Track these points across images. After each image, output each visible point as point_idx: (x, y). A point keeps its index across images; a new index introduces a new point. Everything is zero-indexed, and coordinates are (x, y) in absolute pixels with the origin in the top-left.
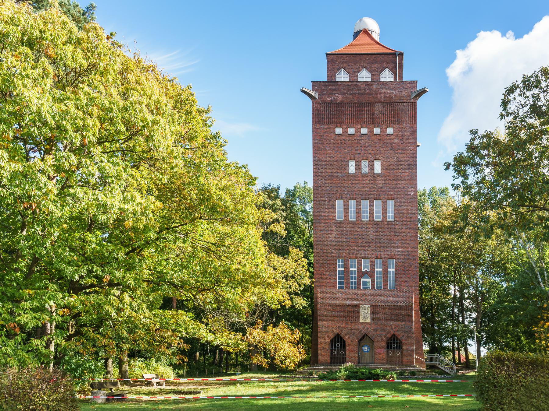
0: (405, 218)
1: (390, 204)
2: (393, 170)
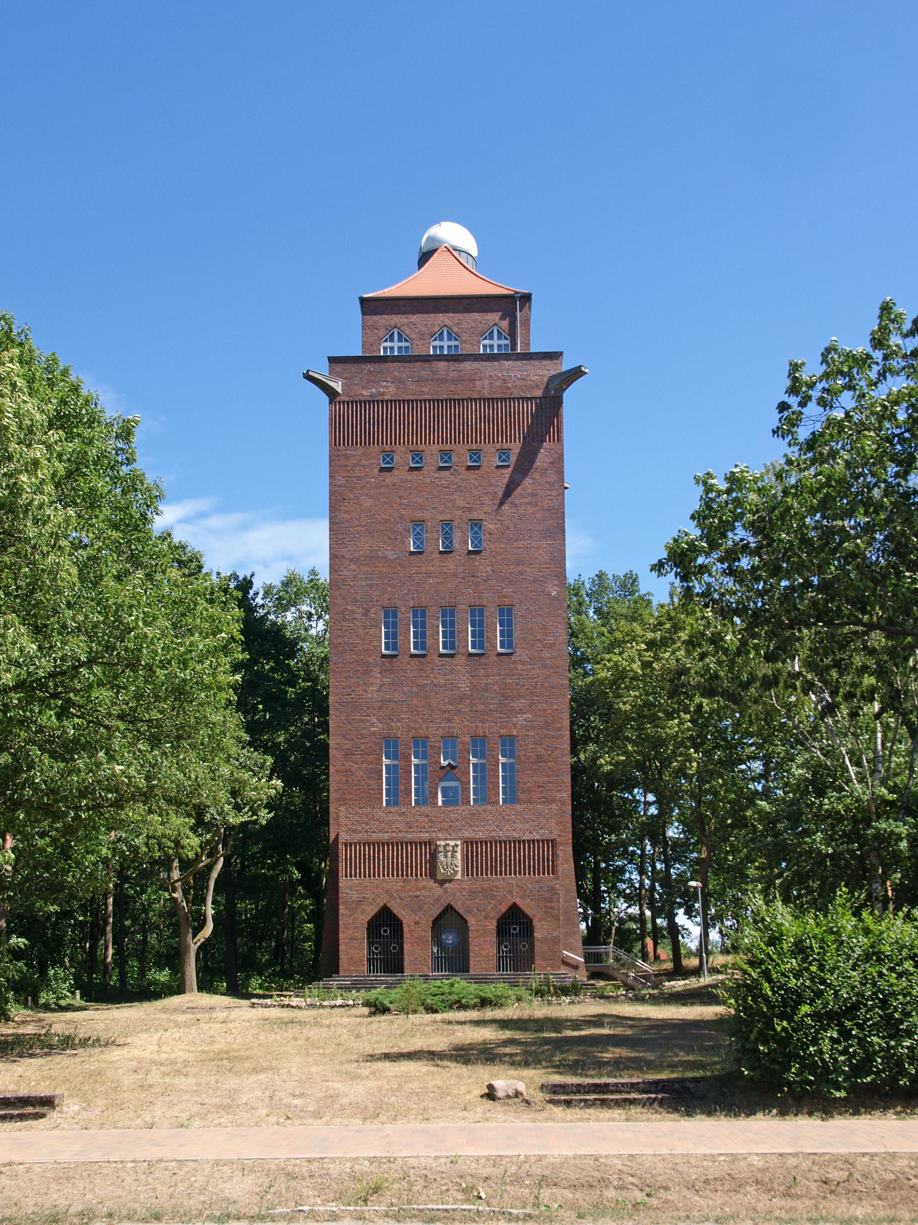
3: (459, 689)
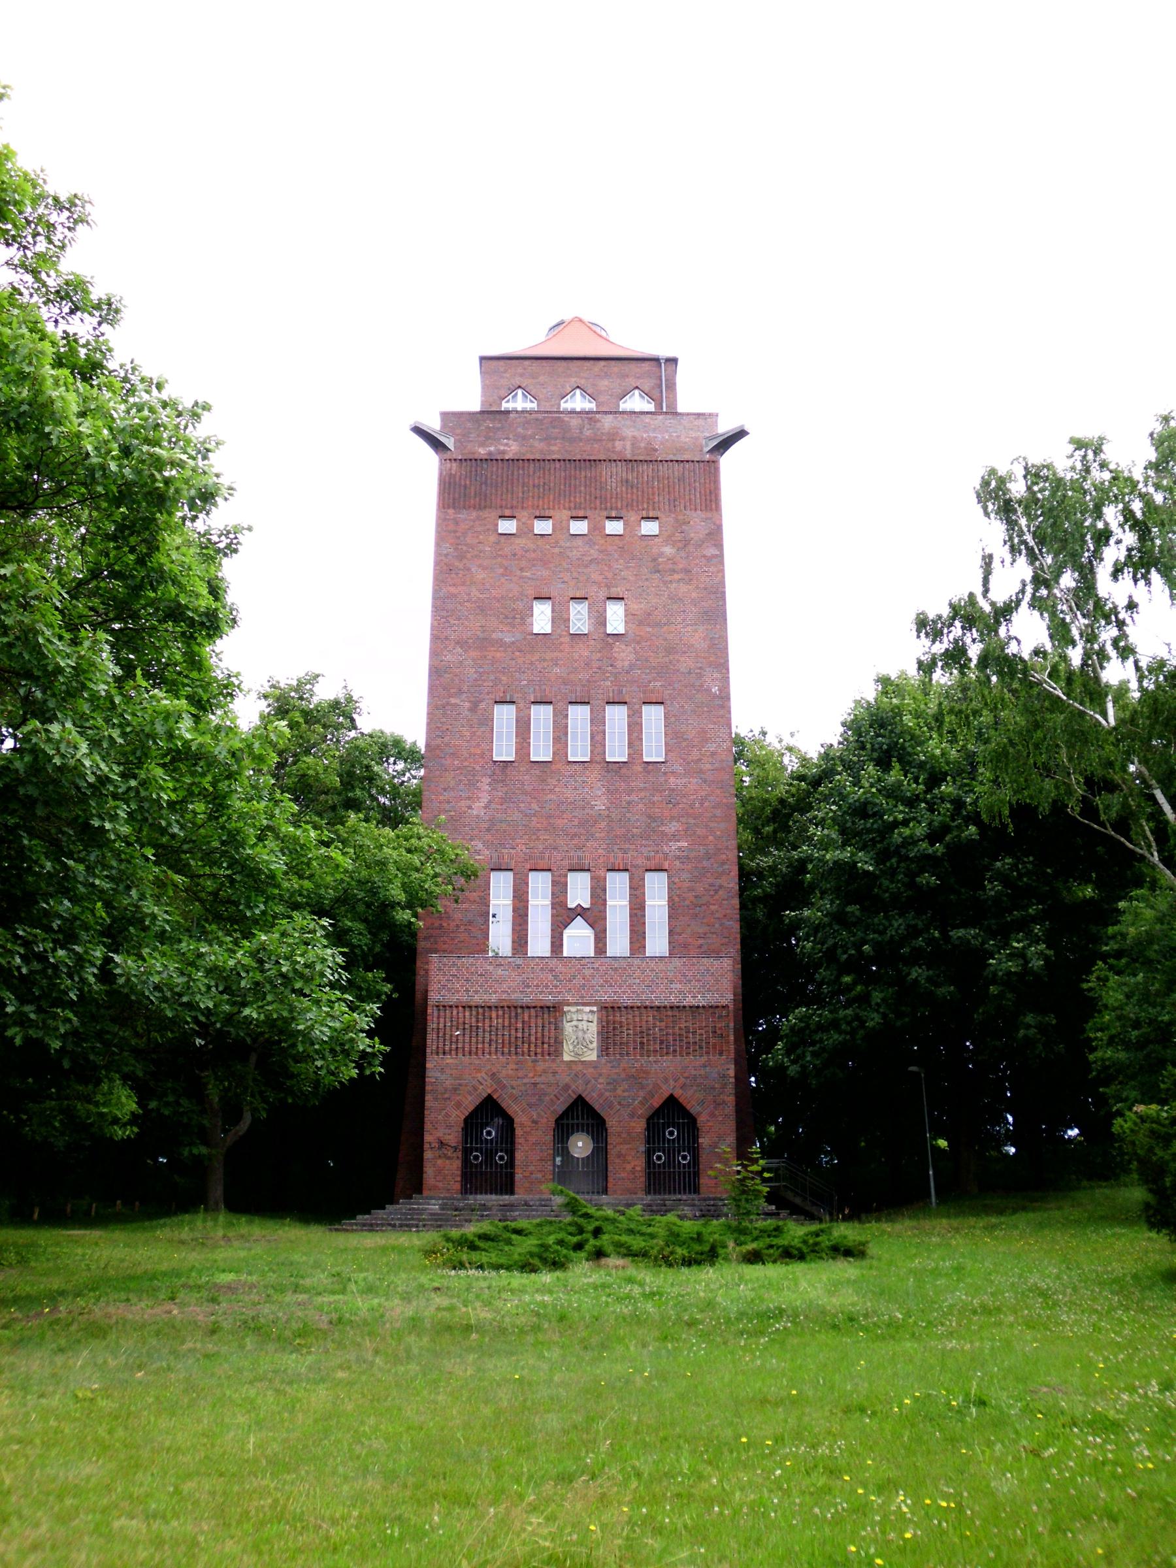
0: (695, 754)
1: (653, 718)
2: (658, 624)
3: (592, 807)
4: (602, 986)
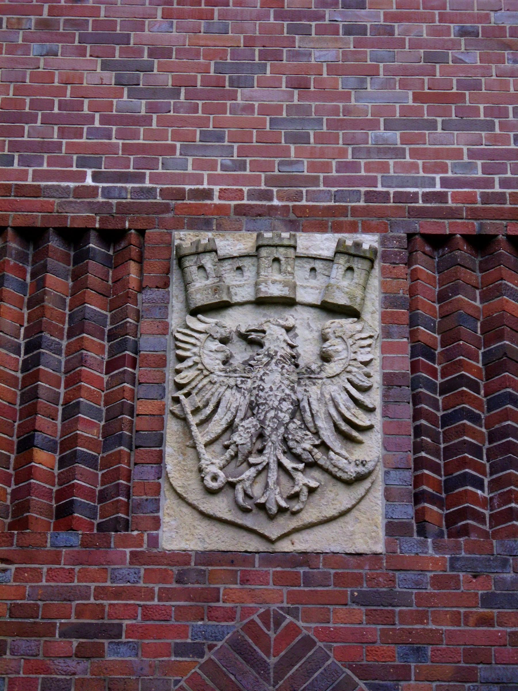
4: (410, 123)
